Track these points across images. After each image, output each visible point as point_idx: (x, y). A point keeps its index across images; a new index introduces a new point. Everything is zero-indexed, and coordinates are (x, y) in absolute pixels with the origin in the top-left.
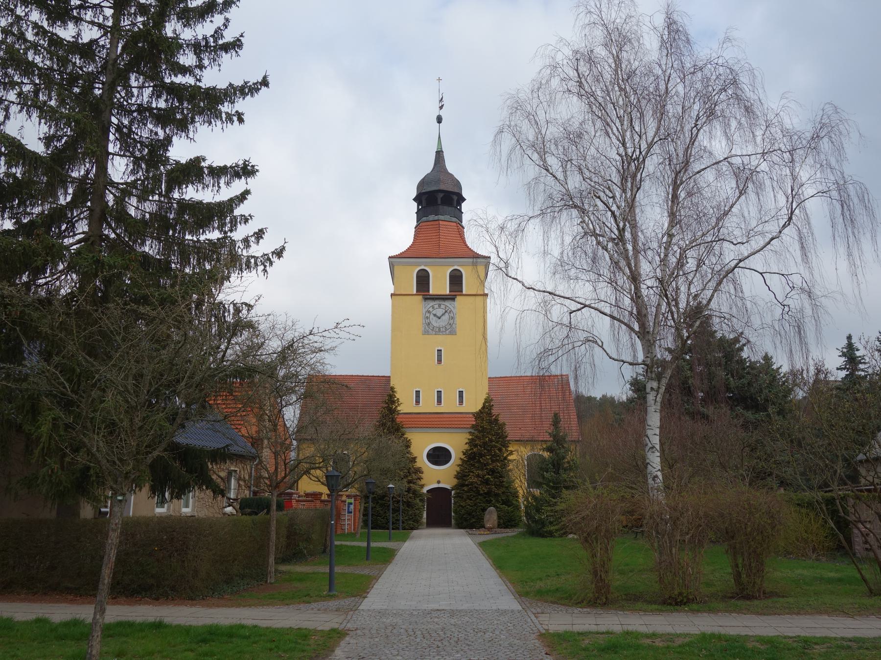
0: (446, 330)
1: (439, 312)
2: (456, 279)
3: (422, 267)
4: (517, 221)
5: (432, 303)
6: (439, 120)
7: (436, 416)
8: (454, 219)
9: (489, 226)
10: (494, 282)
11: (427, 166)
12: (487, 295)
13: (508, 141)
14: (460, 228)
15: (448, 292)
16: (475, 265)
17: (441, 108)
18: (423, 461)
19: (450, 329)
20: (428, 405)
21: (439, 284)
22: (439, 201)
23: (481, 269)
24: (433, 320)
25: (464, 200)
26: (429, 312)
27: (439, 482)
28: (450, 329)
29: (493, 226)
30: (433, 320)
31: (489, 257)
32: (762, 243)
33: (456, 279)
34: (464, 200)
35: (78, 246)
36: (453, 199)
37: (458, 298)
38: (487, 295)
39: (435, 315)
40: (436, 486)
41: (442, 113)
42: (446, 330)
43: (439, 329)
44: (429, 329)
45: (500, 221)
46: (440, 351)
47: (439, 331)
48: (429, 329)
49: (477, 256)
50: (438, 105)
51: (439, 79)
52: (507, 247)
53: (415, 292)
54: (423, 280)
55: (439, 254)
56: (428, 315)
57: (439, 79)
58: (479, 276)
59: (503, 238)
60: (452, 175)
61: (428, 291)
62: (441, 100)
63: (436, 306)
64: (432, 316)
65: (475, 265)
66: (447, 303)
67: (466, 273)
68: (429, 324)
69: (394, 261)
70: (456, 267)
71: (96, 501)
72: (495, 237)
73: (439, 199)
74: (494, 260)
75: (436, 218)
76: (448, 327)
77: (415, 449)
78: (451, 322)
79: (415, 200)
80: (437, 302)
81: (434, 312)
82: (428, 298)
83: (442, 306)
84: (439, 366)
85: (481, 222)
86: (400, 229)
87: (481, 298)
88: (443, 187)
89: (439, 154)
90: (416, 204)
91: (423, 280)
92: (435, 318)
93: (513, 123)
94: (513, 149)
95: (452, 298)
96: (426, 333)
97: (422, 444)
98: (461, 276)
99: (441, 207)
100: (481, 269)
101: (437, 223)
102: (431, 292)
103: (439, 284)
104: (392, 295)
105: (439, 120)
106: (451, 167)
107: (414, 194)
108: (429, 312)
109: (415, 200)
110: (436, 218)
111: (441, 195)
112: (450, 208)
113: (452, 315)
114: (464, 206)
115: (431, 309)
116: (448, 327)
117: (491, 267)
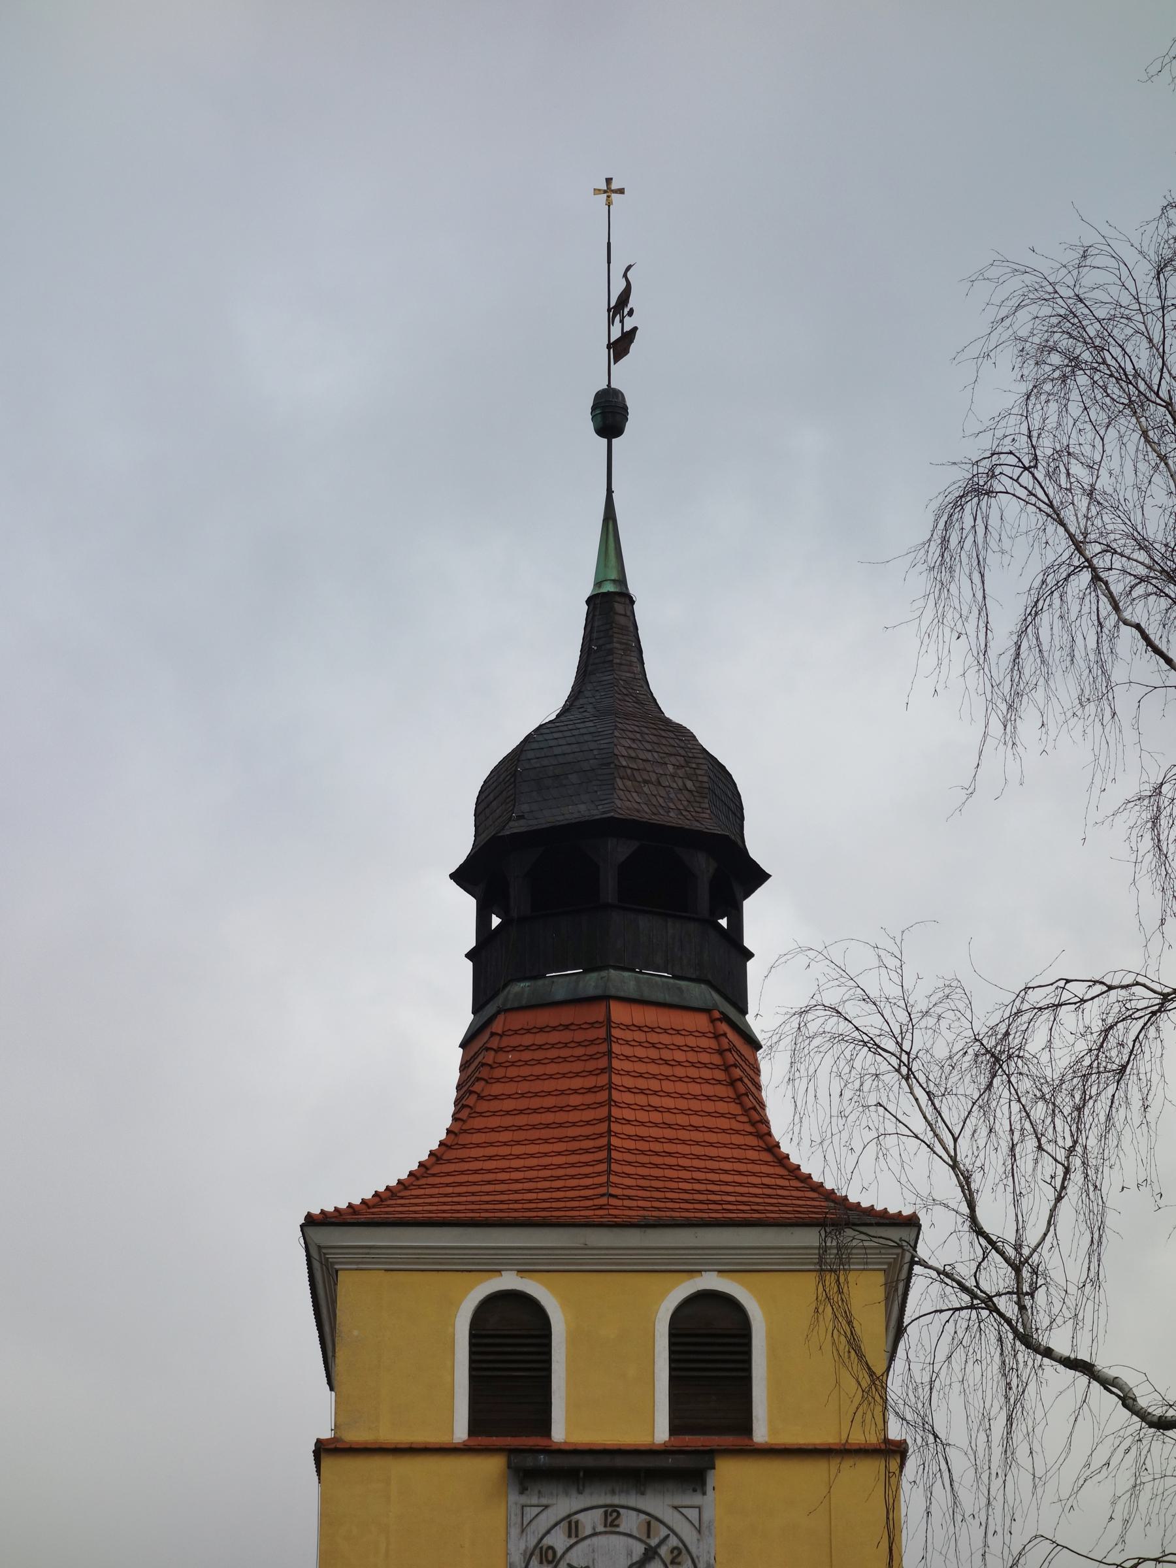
2: (710, 1351)
3: (509, 1281)
4: (1093, 1015)
5: (564, 1504)
6: (610, 415)
8: (698, 993)
9: (919, 1041)
10: (940, 1368)
11: (536, 687)
12: (898, 1451)
13: (1020, 547)
14: (734, 1054)
15: (661, 1434)
16: (830, 1265)
17: (620, 347)
21: (610, 1379)
22: (609, 887)
23: (865, 1290)
25: (756, 877)
29: (937, 1044)
31: (912, 1223)
32: (930, 1118)
33: (710, 1351)
34: (756, 877)
37: (728, 1474)
38: (898, 1451)
41: (627, 377)
45: (987, 1014)
49: (837, 1215)
50: (598, 332)
51: (610, 190)
52: (1025, 1163)
53: (460, 1432)
54: (510, 1352)
55: (607, 1208)
57: (610, 190)
58: (854, 1344)
59: (1005, 1111)
60: (683, 735)
61: (544, 1424)
62: (620, 307)
63: (591, 1521)
65: (830, 1265)
67: (776, 1314)
69: (336, 1243)
70: (711, 1281)
72: (953, 1110)
73: (607, 866)
74: (942, 1241)
75: (591, 983)
79: (461, 877)
83: (630, 1522)
85: (871, 1023)
86: (372, 1024)
87: (868, 1471)
88: (628, 803)
89: (610, 620)
90: (467, 904)
91: (510, 1352)
93: (1046, 447)
94: (1050, 587)
95: (675, 1472)
100: (865, 1290)
101: (595, 1013)
102: (560, 1433)
103: (610, 1379)
104: (322, 1450)
105: (610, 415)
106: (682, 684)
107: (460, 842)
109: (461, 877)
110: (591, 983)
111: (620, 850)
114: (763, 920)
117: (923, 1293)
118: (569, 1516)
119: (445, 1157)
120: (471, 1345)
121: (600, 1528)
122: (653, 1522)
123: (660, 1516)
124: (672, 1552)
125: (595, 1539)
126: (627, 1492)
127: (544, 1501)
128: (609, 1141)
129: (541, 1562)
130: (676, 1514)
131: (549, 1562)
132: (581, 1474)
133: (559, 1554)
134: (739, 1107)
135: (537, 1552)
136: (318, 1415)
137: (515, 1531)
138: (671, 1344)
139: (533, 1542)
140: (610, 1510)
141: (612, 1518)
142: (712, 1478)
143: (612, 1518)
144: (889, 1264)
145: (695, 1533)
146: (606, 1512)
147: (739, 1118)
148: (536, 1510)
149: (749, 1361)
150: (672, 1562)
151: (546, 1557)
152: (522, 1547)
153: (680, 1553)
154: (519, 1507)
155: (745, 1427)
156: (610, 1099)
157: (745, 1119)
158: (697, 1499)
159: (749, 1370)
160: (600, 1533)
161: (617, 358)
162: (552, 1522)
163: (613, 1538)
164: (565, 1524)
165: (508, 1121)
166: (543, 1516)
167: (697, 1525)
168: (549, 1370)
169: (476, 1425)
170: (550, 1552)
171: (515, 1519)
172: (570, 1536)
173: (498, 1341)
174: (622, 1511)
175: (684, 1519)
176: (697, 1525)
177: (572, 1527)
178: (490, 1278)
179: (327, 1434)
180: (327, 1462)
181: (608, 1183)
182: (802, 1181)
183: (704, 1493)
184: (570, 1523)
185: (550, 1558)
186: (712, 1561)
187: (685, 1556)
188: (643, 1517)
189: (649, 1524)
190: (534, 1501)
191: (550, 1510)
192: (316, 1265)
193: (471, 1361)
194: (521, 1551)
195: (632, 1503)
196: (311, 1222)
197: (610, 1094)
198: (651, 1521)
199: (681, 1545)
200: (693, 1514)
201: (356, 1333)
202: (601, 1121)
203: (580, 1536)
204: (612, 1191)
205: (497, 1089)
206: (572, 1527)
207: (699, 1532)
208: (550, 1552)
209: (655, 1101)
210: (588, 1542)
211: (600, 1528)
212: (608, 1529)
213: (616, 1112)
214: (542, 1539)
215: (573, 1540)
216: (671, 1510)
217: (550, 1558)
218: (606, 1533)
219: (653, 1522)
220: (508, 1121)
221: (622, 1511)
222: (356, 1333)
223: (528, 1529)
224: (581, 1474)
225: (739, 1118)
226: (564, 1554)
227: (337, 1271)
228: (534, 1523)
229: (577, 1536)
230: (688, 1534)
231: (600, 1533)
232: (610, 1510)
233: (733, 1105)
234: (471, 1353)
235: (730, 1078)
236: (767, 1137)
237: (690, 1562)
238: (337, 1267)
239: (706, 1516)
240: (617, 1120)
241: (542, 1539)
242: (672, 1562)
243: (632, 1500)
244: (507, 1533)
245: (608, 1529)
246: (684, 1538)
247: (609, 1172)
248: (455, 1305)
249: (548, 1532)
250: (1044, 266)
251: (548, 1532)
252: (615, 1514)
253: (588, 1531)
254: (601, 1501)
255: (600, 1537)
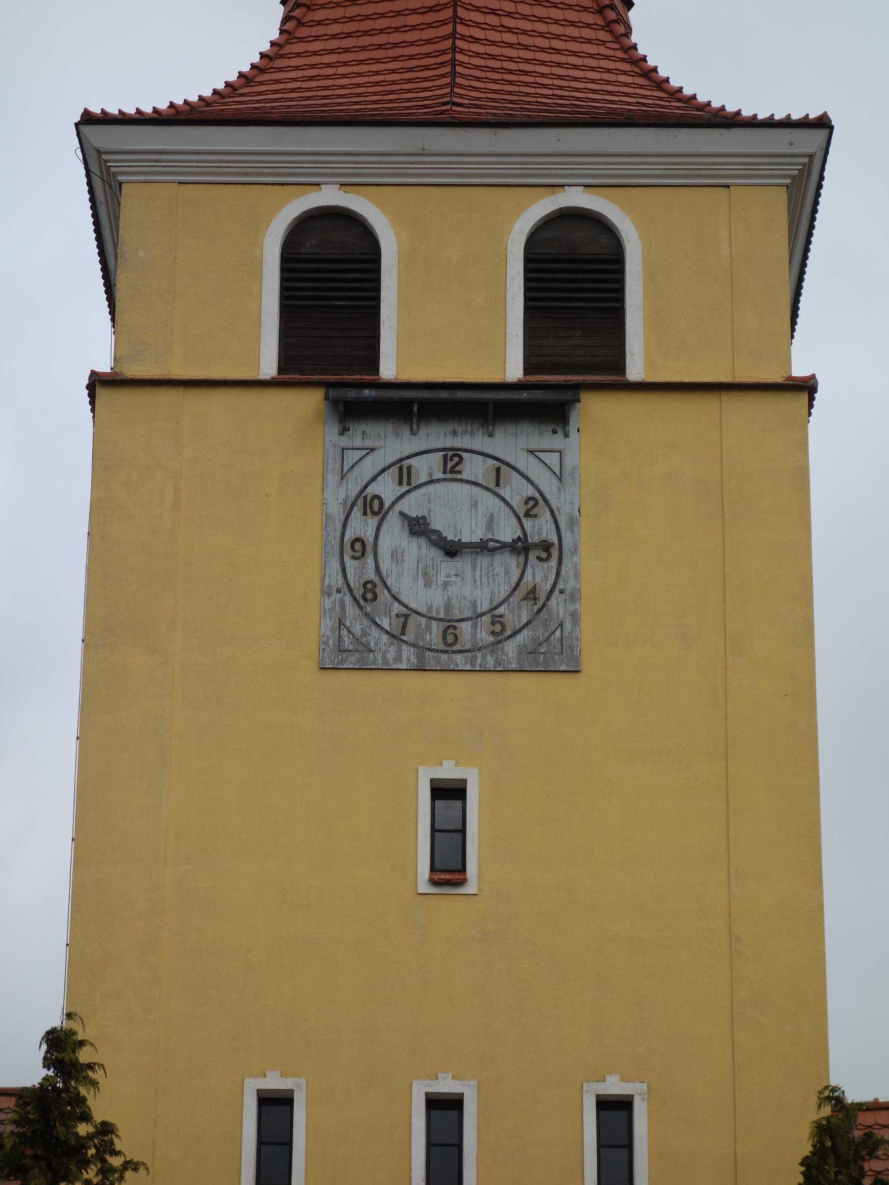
0: (501, 633)
1: (460, 511)
2: (575, 284)
5: (392, 443)
12: (807, 388)
19: (534, 638)
21: (453, 307)
24: (404, 564)
26: (373, 506)
28: (534, 638)
30: (404, 564)
33: (575, 284)
37: (595, 410)
39: (418, 527)
42: (501, 633)
43: (450, 627)
44: (368, 627)
46: (449, 792)
47: (443, 645)
48: (368, 627)
53: (269, 367)
54: (330, 286)
56: (362, 526)
61: (376, 369)
63: (426, 467)
64: (393, 536)
66: (511, 443)
68: (369, 593)
71: (86, 1117)
76: (517, 614)
80: (436, 436)
81: (412, 505)
83: (474, 468)
84: (449, 906)
91: (330, 286)
92: (417, 550)
95: (540, 403)
96: (345, 655)
98: (612, 262)
102: (388, 370)
103: (453, 307)
104: (97, 383)
108: (373, 506)
115: (387, 488)
116: (517, 614)
118: (401, 460)
119: (256, 80)
120: (283, 270)
121: (439, 475)
122: (503, 468)
123: (511, 461)
124: (526, 503)
125: (431, 488)
126: (472, 434)
127: (369, 443)
128: (454, 29)
129: (365, 514)
130: (532, 459)
131: (374, 514)
132: (415, 408)
133: (387, 503)
134: (609, 34)
135: (360, 501)
136: (97, 348)
137: (333, 479)
138: (527, 270)
139: (355, 490)
140: (450, 453)
141: (453, 461)
142: (576, 418)
143: (453, 461)
144: (793, 178)
145: (555, 481)
146: (445, 457)
147: (608, 45)
148: (359, 454)
149: (621, 290)
150: (527, 515)
151: (371, 507)
152: (342, 496)
153: (536, 504)
154: (340, 451)
155: (617, 363)
156: (455, 15)
157: (617, 46)
158: (557, 442)
159: (621, 300)
160: (438, 481)
162: (379, 468)
163: (455, 486)
164: (395, 470)
165: (333, 44)
166: (368, 461)
167: (558, 473)
168: (377, 299)
169: (286, 361)
170: (376, 502)
171: (334, 464)
172: (400, 483)
173: (314, 266)
174: (464, 455)
175: (541, 464)
176: (558, 473)
177: (403, 473)
178: (306, 193)
179: (105, 366)
180: (101, 393)
181: (453, 35)
182: (684, 102)
183: (566, 436)
184: (401, 468)
185: (376, 509)
186: (576, 513)
187: (542, 507)
188: (491, 462)
189: (498, 470)
190: (358, 443)
191: (376, 454)
192: (97, 182)
193: (283, 289)
194: (341, 501)
195: (477, 447)
196: (88, 119)
197: (455, 11)
198: (501, 468)
199: (537, 495)
200: (553, 459)
201: (142, 254)
202: (444, 38)
203: (413, 484)
204: (455, 100)
205: (320, 15)
206: (403, 473)
207: (560, 480)
208: (376, 502)
209: (508, 22)
210: (423, 490)
211: (439, 475)
212: (448, 476)
213: (460, 29)
214: (366, 486)
215: (405, 488)
216: (525, 455)
217: (376, 509)
218: (445, 480)
219: (503, 468)
220: (333, 44)
221: (464, 455)
222: (142, 254)
223: (350, 475)
224: (415, 408)
225: (608, 45)
226: (393, 504)
227: (120, 184)
228: (356, 469)
229: (409, 484)
231: (438, 481)
232: (450, 453)
233: (601, 32)
234: (283, 279)
235: (598, 5)
236: (643, 63)
237: (548, 514)
238: (121, 178)
239: (568, 462)
240: (463, 38)
241: (366, 486)
242: (527, 515)
243: (477, 440)
244: (324, 480)
245: (448, 476)
246: (542, 487)
247: (453, 85)
248: (263, 223)
249: (374, 479)
251: (374, 479)
252: (456, 459)
253: (424, 478)
254: (440, 444)
255: (438, 485)
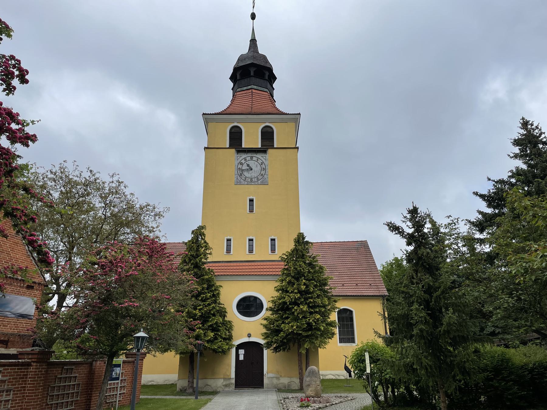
0: (258, 180)
2: (267, 135)
5: (244, 156)
7: (247, 264)
11: (245, 49)
15: (260, 146)
18: (233, 314)
19: (262, 180)
20: (240, 253)
21: (251, 138)
22: (252, 74)
27: (249, 336)
28: (262, 180)
33: (267, 135)
35: (387, 324)
36: (264, 74)
40: (246, 340)
42: (258, 180)
43: (251, 179)
53: (228, 146)
54: (236, 136)
63: (248, 159)
66: (259, 156)
76: (260, 177)
77: (223, 299)
78: (263, 172)
82: (241, 151)
83: (254, 159)
84: (251, 214)
89: (253, 42)
91: (236, 136)
95: (262, 151)
97: (231, 294)
98: (272, 132)
99: (253, 79)
101: (250, 91)
102: (243, 146)
103: (251, 138)
104: (205, 148)
105: (253, 16)
112: (262, 81)
113: (263, 166)
115: (243, 161)
116: (260, 177)
158: (265, 155)
161: (201, 228)
169: (230, 145)
177: (245, 160)
206: (245, 160)
230: (264, 161)
250: (183, 252)
